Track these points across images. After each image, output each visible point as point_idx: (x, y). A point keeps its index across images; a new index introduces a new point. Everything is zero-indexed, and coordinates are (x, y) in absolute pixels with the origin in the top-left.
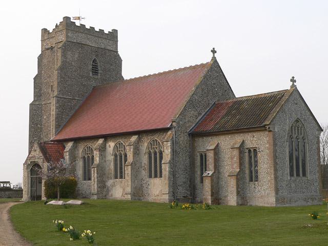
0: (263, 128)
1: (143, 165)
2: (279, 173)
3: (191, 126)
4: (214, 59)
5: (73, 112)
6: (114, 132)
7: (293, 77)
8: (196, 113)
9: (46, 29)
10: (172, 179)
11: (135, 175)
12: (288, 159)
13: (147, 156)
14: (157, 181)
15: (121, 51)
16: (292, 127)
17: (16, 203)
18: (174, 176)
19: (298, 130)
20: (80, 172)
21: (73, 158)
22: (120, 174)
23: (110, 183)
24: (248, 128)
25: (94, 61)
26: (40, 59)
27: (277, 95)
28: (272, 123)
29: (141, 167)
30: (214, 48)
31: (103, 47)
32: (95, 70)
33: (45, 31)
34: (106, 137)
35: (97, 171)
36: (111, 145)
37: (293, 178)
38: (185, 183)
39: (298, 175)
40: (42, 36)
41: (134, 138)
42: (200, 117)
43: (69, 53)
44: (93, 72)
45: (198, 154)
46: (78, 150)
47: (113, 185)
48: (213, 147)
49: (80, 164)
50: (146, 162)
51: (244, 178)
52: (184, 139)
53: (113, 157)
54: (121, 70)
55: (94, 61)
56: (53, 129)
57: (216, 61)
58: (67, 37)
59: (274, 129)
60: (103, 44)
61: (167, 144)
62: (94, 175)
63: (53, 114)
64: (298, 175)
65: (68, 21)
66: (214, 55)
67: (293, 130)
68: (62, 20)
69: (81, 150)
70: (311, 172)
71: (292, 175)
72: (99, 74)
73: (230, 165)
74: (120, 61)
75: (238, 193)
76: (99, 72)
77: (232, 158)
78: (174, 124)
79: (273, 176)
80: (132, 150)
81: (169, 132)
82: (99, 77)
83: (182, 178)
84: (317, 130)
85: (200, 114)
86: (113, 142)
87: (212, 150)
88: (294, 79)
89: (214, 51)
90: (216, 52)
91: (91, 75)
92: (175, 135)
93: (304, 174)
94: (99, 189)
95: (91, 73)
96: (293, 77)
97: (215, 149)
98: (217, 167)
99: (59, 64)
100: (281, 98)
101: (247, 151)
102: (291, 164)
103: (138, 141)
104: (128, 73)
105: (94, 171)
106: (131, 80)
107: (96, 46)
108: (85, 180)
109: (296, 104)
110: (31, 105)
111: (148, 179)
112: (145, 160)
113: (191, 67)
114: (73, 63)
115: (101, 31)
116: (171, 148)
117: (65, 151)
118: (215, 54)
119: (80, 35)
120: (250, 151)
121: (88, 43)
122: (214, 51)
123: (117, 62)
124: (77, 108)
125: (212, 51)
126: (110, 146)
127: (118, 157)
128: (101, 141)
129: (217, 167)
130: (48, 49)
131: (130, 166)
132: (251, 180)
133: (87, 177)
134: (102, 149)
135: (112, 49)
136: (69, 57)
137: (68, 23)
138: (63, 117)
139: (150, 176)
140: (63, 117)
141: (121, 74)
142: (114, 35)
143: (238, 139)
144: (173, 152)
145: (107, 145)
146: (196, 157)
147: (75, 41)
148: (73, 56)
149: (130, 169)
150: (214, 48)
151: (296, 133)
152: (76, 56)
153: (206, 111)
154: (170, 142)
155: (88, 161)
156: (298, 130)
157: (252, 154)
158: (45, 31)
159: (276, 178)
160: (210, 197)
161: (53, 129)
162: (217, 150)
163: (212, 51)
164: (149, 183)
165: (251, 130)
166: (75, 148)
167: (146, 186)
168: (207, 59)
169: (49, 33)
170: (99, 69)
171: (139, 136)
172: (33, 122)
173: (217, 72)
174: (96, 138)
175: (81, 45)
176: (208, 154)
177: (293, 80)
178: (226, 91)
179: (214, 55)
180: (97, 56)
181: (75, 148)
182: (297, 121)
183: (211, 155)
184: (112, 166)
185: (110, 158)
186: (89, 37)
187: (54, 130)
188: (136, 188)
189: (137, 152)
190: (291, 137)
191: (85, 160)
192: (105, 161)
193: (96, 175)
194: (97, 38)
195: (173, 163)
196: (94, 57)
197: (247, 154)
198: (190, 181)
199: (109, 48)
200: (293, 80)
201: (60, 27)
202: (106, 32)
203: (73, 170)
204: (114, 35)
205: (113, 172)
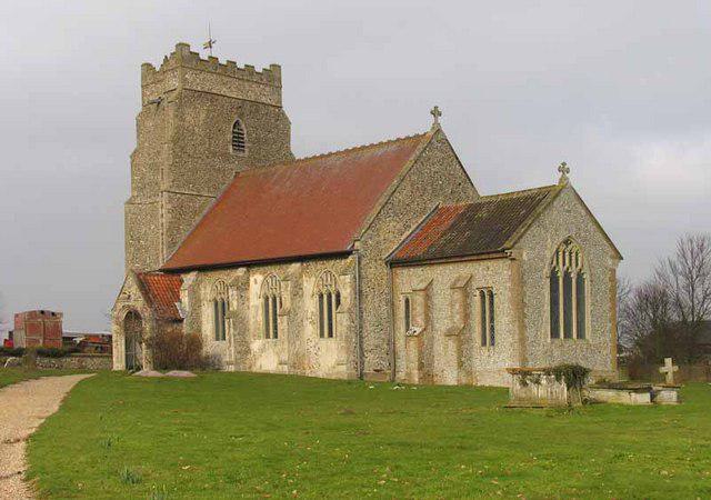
0: (501, 254)
2: (530, 333)
5: (198, 219)
6: (262, 258)
7: (564, 164)
9: (150, 65)
15: (287, 108)
16: (557, 252)
17: (83, 376)
19: (571, 257)
20: (208, 328)
21: (196, 302)
23: (256, 345)
27: (532, 198)
28: (516, 246)
32: (238, 142)
33: (148, 67)
37: (556, 341)
39: (568, 335)
40: (144, 77)
42: (408, 233)
43: (188, 110)
48: (422, 286)
51: (470, 340)
57: (439, 131)
58: (185, 81)
64: (568, 335)
65: (186, 52)
68: (174, 50)
71: (554, 334)
73: (446, 315)
74: (287, 123)
77: (452, 306)
78: (357, 244)
79: (517, 337)
81: (350, 258)
82: (247, 153)
84: (612, 257)
87: (420, 290)
89: (436, 113)
91: (231, 150)
93: (581, 335)
94: (239, 356)
96: (564, 164)
97: (425, 289)
98: (428, 320)
99: (170, 133)
100: (540, 200)
101: (478, 293)
102: (554, 318)
108: (217, 339)
118: (440, 119)
121: (224, 91)
122: (436, 113)
123: (276, 123)
126: (256, 282)
129: (428, 320)
131: (422, 293)
132: (484, 344)
137: (185, 58)
141: (288, 148)
142: (272, 77)
145: (252, 279)
148: (197, 116)
149: (285, 324)
151: (567, 261)
152: (203, 116)
156: (571, 257)
157: (221, 334)
159: (522, 340)
162: (427, 291)
169: (155, 73)
173: (442, 151)
174: (234, 266)
175: (211, 96)
180: (241, 115)
182: (567, 242)
183: (419, 298)
186: (226, 79)
193: (232, 330)
194: (241, 82)
197: (477, 299)
199: (263, 99)
200: (563, 169)
201: (172, 62)
202: (259, 69)
203: (197, 320)
204: (272, 77)
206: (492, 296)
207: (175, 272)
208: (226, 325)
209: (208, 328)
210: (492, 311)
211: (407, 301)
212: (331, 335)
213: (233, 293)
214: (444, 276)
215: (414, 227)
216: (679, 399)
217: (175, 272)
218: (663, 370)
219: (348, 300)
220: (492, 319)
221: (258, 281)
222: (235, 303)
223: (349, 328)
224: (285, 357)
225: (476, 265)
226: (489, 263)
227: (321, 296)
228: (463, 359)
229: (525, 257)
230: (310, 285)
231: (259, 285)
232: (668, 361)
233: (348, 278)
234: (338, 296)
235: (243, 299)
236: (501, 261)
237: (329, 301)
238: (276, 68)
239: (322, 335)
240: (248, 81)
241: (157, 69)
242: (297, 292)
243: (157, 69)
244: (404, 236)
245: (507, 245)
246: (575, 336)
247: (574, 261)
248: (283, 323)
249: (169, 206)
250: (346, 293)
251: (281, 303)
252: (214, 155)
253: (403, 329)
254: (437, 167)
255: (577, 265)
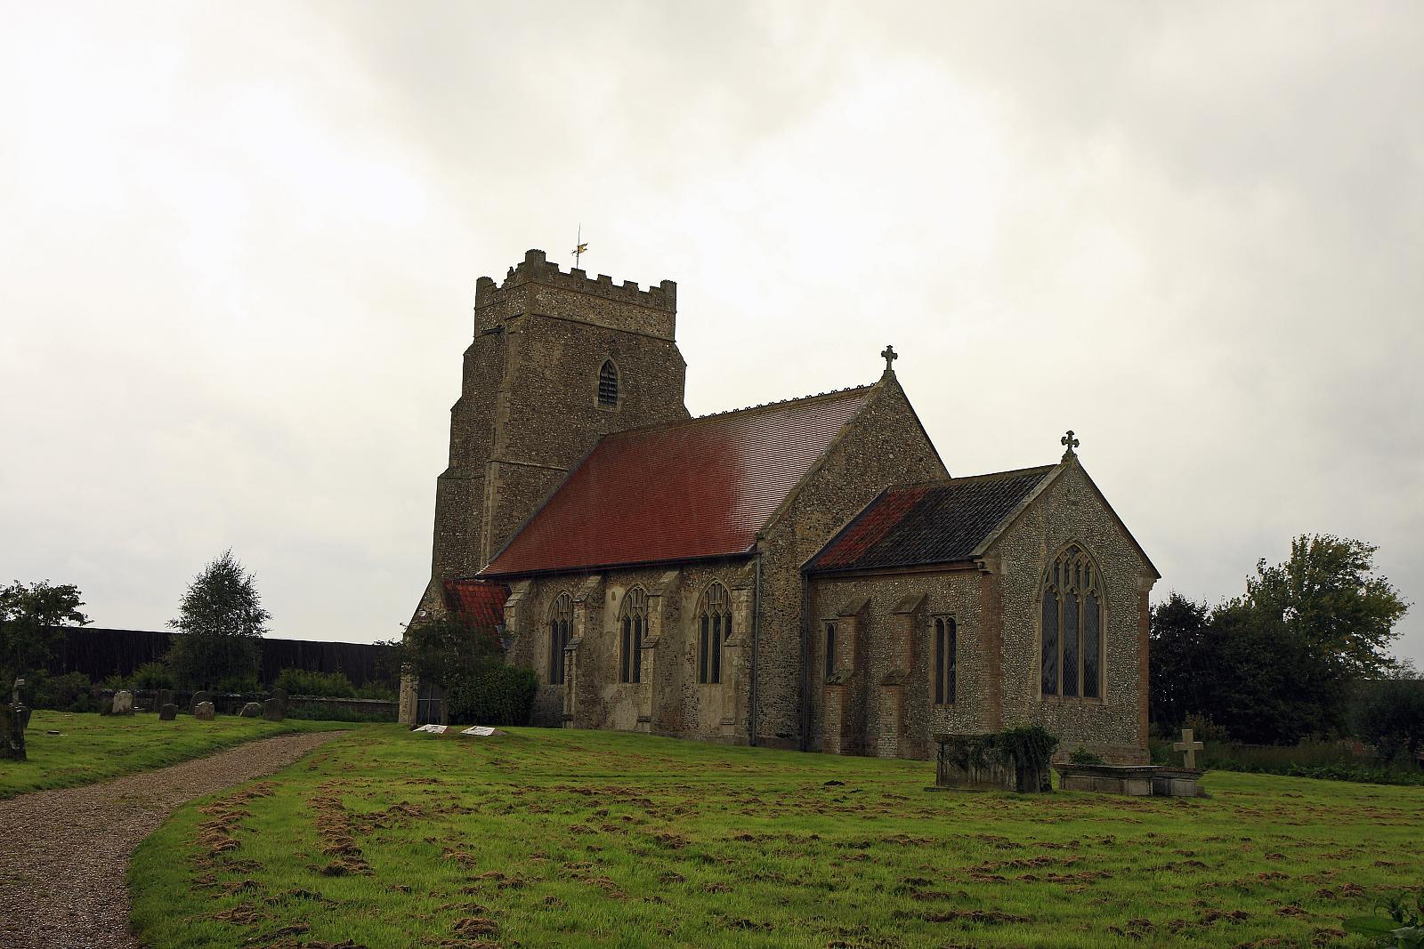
0: (971, 565)
1: (687, 649)
2: (1008, 684)
3: (808, 553)
4: (889, 375)
7: (1070, 433)
8: (828, 519)
10: (748, 688)
11: (667, 676)
12: (1037, 648)
13: (697, 626)
14: (716, 691)
15: (684, 340)
18: (753, 679)
20: (542, 664)
21: (528, 623)
22: (630, 672)
23: (610, 691)
24: (936, 563)
25: (607, 367)
26: (471, 357)
29: (684, 654)
30: (890, 347)
31: (633, 328)
32: (608, 392)
33: (484, 284)
34: (607, 573)
35: (578, 660)
36: (617, 591)
37: (1051, 699)
38: (783, 698)
39: (1070, 690)
41: (669, 577)
42: (839, 529)
44: (613, 392)
45: (823, 626)
46: (541, 603)
47: (617, 699)
49: (544, 639)
50: (695, 642)
52: (785, 585)
53: (619, 625)
54: (682, 393)
55: (607, 367)
56: (485, 544)
59: (999, 568)
60: (633, 320)
61: (739, 597)
62: (572, 671)
63: (487, 509)
66: (889, 365)
67: (1061, 572)
69: (546, 606)
70: (1112, 687)
71: (1048, 689)
72: (619, 403)
73: (893, 654)
74: (681, 365)
75: (904, 729)
76: (620, 395)
78: (761, 544)
80: (659, 608)
83: (775, 686)
85: (837, 521)
86: (622, 585)
88: (1074, 438)
89: (889, 355)
90: (895, 356)
92: (762, 573)
95: (596, 399)
96: (1070, 433)
101: (933, 622)
103: (678, 588)
104: (701, 399)
105: (571, 661)
106: (703, 418)
107: (615, 327)
109: (1074, 503)
110: (442, 479)
111: (696, 686)
112: (692, 635)
113: (795, 400)
114: (547, 372)
115: (630, 287)
116: (747, 607)
117: (508, 604)
119: (569, 297)
120: (939, 622)
121: (591, 317)
122: (889, 355)
123: (673, 368)
124: (553, 490)
125: (883, 354)
126: (614, 598)
127: (633, 624)
128: (593, 581)
130: (489, 333)
132: (939, 700)
133: (557, 675)
134: (594, 604)
135: (657, 333)
136: (536, 356)
137: (535, 266)
138: (515, 514)
139: (703, 680)
140: (515, 514)
142: (666, 294)
143: (914, 587)
144: (754, 618)
145: (609, 593)
146: (817, 634)
147: (555, 314)
149: (651, 659)
150: (890, 347)
152: (557, 353)
153: (858, 513)
154: (745, 592)
155: (562, 633)
158: (484, 284)
160: (838, 738)
161: (485, 544)
162: (863, 617)
163: (883, 354)
164: (698, 695)
165: (944, 568)
166: (532, 598)
167: (692, 704)
168: (871, 374)
170: (620, 387)
171: (681, 572)
172: (445, 526)
173: (893, 409)
174: (577, 573)
176: (842, 626)
177: (1069, 440)
178: (921, 460)
179: (889, 365)
180: (614, 353)
181: (532, 598)
183: (847, 629)
184: (617, 650)
185: (614, 627)
187: (488, 549)
188: (665, 708)
189: (673, 612)
190: (1051, 593)
191: (555, 630)
192: (601, 635)
195: (752, 646)
196: (607, 356)
197: (933, 630)
198: (800, 696)
199: (649, 331)
200: (1069, 440)
204: (666, 294)
205: (618, 664)
206: (952, 625)
207: (502, 582)
208: (567, 662)
209: (542, 664)
210: (953, 650)
211: (831, 631)
212: (716, 680)
213: (580, 612)
214: (886, 593)
215: (847, 521)
216: (25, 681)
217: (502, 582)
218: (1177, 746)
219: (743, 627)
220: (952, 662)
221: (617, 594)
222: (581, 628)
223: (741, 669)
224: (647, 710)
225: (933, 580)
226: (953, 578)
227: (705, 621)
228: (907, 722)
229: (1004, 570)
230: (691, 603)
231: (617, 603)
232: (1188, 733)
233: (744, 595)
234: (729, 619)
235: (595, 621)
236: (967, 577)
237: (716, 626)
238: (668, 290)
239: (703, 680)
240: (627, 303)
241: (499, 286)
242: (673, 612)
243: (499, 286)
244: (831, 536)
245: (978, 551)
246: (1081, 692)
247: (1061, 577)
248: (648, 661)
249: (500, 483)
250: (741, 616)
251: (647, 630)
252: (570, 408)
253: (822, 673)
254: (887, 434)
255: (1066, 583)
